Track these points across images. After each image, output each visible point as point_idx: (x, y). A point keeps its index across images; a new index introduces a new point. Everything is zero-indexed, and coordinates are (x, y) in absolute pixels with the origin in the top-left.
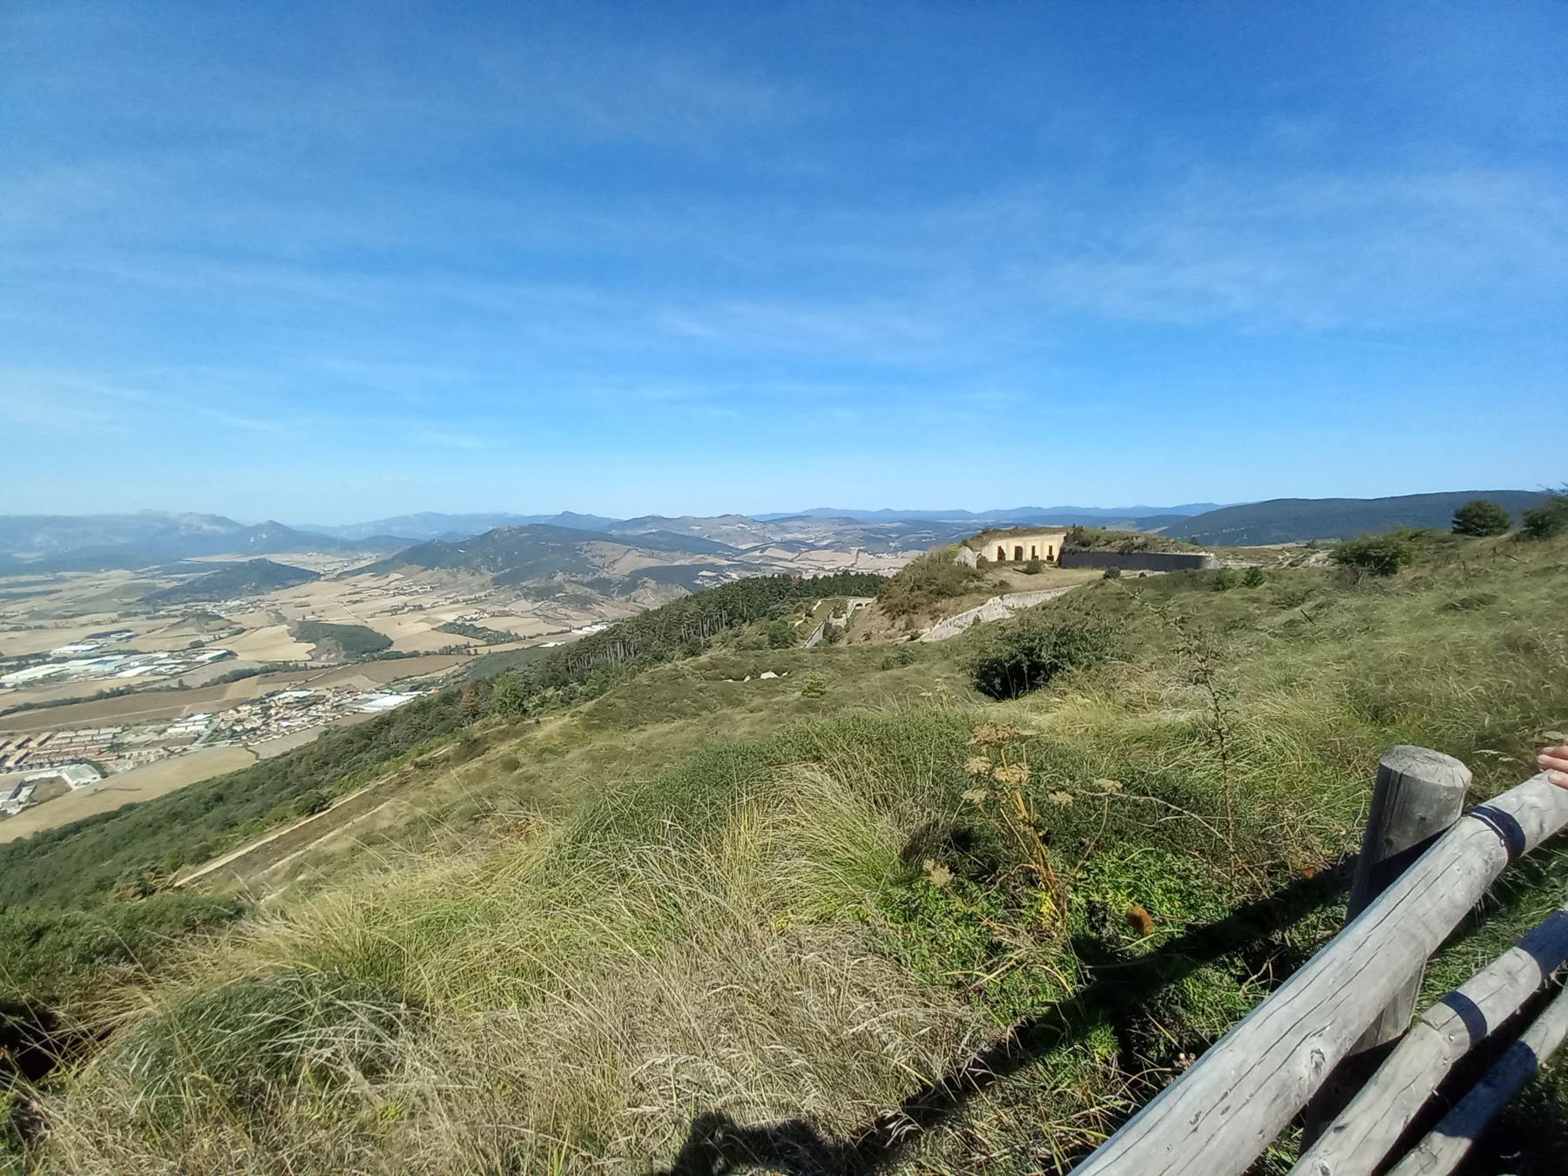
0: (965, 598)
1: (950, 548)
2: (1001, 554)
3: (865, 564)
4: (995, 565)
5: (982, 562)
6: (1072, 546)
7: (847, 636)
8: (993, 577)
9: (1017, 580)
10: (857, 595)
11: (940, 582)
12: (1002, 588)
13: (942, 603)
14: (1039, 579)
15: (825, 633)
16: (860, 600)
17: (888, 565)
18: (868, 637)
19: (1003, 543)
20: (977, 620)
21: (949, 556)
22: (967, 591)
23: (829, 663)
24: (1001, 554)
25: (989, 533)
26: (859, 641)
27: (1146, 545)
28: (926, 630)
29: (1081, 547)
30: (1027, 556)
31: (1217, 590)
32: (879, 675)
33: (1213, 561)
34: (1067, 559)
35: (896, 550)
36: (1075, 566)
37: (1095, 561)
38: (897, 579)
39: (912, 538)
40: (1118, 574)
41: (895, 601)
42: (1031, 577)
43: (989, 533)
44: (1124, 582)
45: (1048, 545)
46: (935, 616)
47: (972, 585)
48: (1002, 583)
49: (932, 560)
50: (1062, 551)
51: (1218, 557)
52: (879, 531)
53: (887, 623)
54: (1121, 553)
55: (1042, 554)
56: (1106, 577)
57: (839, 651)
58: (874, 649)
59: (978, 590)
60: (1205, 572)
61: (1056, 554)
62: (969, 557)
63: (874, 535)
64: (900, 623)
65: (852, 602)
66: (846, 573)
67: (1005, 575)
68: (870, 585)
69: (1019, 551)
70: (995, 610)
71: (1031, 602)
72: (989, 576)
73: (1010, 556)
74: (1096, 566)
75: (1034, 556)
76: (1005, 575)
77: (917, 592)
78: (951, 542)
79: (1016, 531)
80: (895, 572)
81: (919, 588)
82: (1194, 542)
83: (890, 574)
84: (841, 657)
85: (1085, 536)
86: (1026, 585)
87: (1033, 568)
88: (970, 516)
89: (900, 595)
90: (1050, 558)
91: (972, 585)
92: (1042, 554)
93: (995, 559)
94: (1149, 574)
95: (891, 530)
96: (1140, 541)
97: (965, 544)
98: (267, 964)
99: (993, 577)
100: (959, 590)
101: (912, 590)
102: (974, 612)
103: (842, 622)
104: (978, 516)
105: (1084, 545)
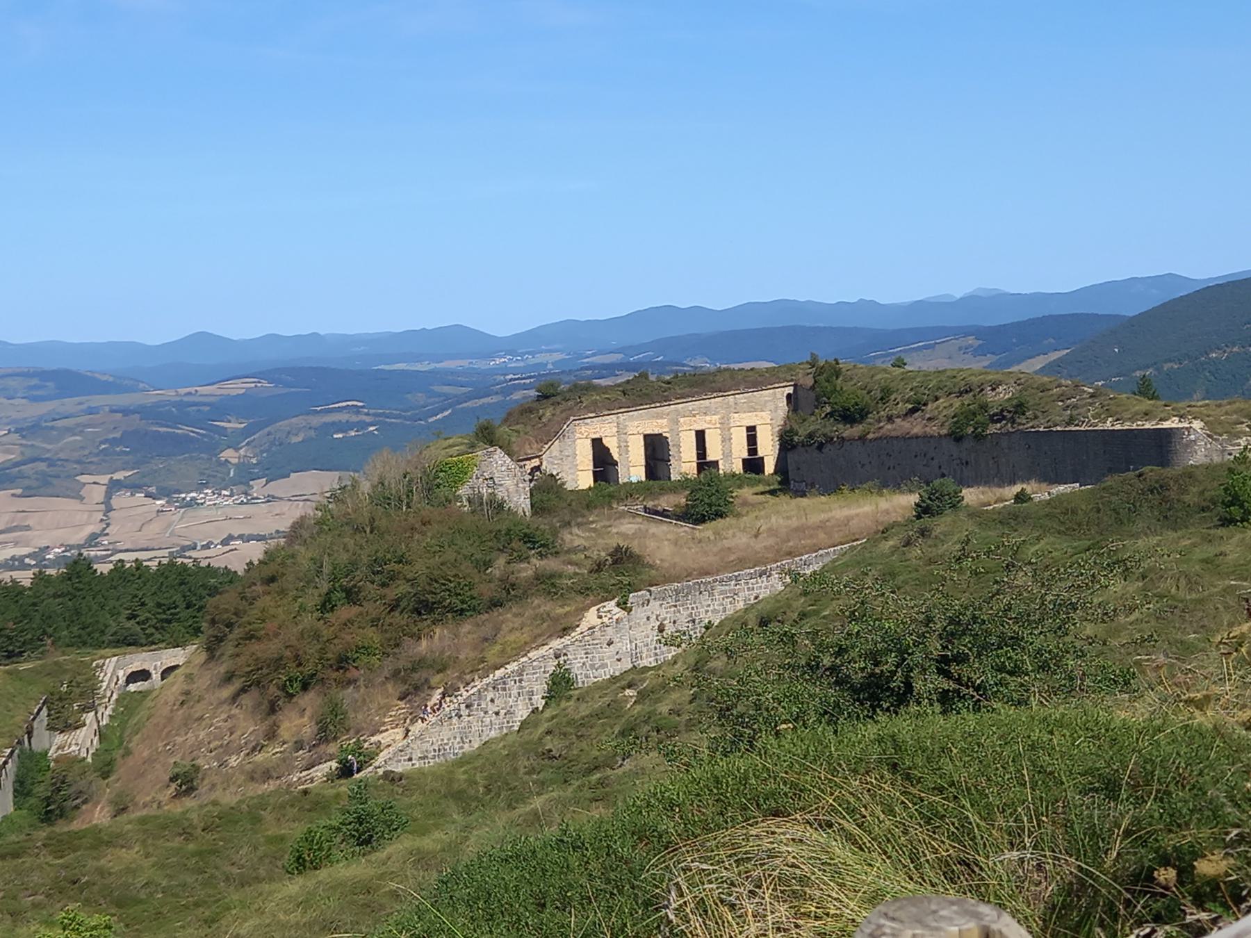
0: (508, 617)
1: (437, 452)
2: (603, 461)
3: (140, 530)
4: (586, 502)
5: (547, 491)
6: (815, 424)
7: (107, 790)
8: (587, 539)
9: (663, 542)
10: (127, 642)
11: (420, 568)
12: (622, 574)
13: (437, 640)
14: (731, 534)
15: (22, 790)
16: (139, 660)
17: (229, 527)
18: (186, 782)
19: (605, 428)
20: (560, 684)
21: (437, 482)
22: (510, 593)
23: (68, 887)
24: (603, 461)
25: (556, 397)
26: (154, 796)
27: (1020, 408)
28: (391, 737)
29: (848, 415)
30: (684, 463)
31: (1227, 522)
32: (294, 886)
33: (1201, 443)
34: (804, 465)
35: (245, 477)
36: (831, 487)
37: (885, 466)
38: (269, 573)
39: (296, 429)
40: (956, 504)
41: (271, 648)
42: (706, 531)
43: (556, 397)
44: (975, 514)
45: (741, 426)
46: (413, 686)
47: (525, 571)
48: (623, 559)
49: (383, 499)
50: (787, 443)
51: (1214, 429)
52: (182, 412)
53: (250, 728)
54: (956, 437)
55: (729, 455)
56: (923, 510)
57: (100, 841)
58: (225, 819)
59: (547, 584)
60: (1190, 474)
61: (768, 450)
62: (503, 478)
63: (165, 423)
64: (297, 722)
65: (113, 670)
66: (78, 568)
67: (627, 528)
68: (173, 601)
69: (656, 449)
70: (616, 642)
71: (717, 605)
72: (574, 537)
73: (633, 469)
74: (891, 481)
75: (704, 464)
76: (627, 528)
77: (346, 612)
78: (439, 432)
79: (641, 389)
80: (255, 552)
81: (352, 596)
82: (1145, 389)
83: (242, 557)
84: (116, 860)
85: (849, 391)
86: (691, 556)
87: (707, 500)
88: (488, 345)
89: (289, 623)
90: (753, 464)
91: (525, 571)
92: (729, 455)
93: (584, 479)
94: (1041, 493)
95: (223, 408)
96: (1003, 395)
97: (487, 436)
98: (1025, 772)
99: (587, 539)
100: (487, 591)
101: (327, 605)
102: (539, 663)
103: (81, 742)
104: (512, 345)
105: (848, 416)
